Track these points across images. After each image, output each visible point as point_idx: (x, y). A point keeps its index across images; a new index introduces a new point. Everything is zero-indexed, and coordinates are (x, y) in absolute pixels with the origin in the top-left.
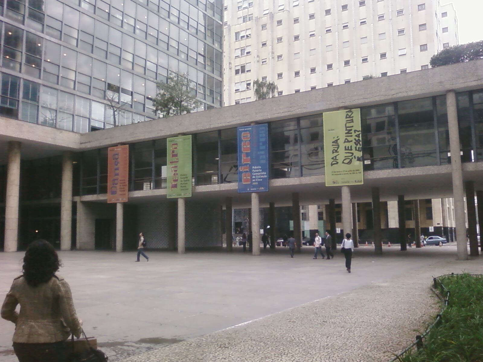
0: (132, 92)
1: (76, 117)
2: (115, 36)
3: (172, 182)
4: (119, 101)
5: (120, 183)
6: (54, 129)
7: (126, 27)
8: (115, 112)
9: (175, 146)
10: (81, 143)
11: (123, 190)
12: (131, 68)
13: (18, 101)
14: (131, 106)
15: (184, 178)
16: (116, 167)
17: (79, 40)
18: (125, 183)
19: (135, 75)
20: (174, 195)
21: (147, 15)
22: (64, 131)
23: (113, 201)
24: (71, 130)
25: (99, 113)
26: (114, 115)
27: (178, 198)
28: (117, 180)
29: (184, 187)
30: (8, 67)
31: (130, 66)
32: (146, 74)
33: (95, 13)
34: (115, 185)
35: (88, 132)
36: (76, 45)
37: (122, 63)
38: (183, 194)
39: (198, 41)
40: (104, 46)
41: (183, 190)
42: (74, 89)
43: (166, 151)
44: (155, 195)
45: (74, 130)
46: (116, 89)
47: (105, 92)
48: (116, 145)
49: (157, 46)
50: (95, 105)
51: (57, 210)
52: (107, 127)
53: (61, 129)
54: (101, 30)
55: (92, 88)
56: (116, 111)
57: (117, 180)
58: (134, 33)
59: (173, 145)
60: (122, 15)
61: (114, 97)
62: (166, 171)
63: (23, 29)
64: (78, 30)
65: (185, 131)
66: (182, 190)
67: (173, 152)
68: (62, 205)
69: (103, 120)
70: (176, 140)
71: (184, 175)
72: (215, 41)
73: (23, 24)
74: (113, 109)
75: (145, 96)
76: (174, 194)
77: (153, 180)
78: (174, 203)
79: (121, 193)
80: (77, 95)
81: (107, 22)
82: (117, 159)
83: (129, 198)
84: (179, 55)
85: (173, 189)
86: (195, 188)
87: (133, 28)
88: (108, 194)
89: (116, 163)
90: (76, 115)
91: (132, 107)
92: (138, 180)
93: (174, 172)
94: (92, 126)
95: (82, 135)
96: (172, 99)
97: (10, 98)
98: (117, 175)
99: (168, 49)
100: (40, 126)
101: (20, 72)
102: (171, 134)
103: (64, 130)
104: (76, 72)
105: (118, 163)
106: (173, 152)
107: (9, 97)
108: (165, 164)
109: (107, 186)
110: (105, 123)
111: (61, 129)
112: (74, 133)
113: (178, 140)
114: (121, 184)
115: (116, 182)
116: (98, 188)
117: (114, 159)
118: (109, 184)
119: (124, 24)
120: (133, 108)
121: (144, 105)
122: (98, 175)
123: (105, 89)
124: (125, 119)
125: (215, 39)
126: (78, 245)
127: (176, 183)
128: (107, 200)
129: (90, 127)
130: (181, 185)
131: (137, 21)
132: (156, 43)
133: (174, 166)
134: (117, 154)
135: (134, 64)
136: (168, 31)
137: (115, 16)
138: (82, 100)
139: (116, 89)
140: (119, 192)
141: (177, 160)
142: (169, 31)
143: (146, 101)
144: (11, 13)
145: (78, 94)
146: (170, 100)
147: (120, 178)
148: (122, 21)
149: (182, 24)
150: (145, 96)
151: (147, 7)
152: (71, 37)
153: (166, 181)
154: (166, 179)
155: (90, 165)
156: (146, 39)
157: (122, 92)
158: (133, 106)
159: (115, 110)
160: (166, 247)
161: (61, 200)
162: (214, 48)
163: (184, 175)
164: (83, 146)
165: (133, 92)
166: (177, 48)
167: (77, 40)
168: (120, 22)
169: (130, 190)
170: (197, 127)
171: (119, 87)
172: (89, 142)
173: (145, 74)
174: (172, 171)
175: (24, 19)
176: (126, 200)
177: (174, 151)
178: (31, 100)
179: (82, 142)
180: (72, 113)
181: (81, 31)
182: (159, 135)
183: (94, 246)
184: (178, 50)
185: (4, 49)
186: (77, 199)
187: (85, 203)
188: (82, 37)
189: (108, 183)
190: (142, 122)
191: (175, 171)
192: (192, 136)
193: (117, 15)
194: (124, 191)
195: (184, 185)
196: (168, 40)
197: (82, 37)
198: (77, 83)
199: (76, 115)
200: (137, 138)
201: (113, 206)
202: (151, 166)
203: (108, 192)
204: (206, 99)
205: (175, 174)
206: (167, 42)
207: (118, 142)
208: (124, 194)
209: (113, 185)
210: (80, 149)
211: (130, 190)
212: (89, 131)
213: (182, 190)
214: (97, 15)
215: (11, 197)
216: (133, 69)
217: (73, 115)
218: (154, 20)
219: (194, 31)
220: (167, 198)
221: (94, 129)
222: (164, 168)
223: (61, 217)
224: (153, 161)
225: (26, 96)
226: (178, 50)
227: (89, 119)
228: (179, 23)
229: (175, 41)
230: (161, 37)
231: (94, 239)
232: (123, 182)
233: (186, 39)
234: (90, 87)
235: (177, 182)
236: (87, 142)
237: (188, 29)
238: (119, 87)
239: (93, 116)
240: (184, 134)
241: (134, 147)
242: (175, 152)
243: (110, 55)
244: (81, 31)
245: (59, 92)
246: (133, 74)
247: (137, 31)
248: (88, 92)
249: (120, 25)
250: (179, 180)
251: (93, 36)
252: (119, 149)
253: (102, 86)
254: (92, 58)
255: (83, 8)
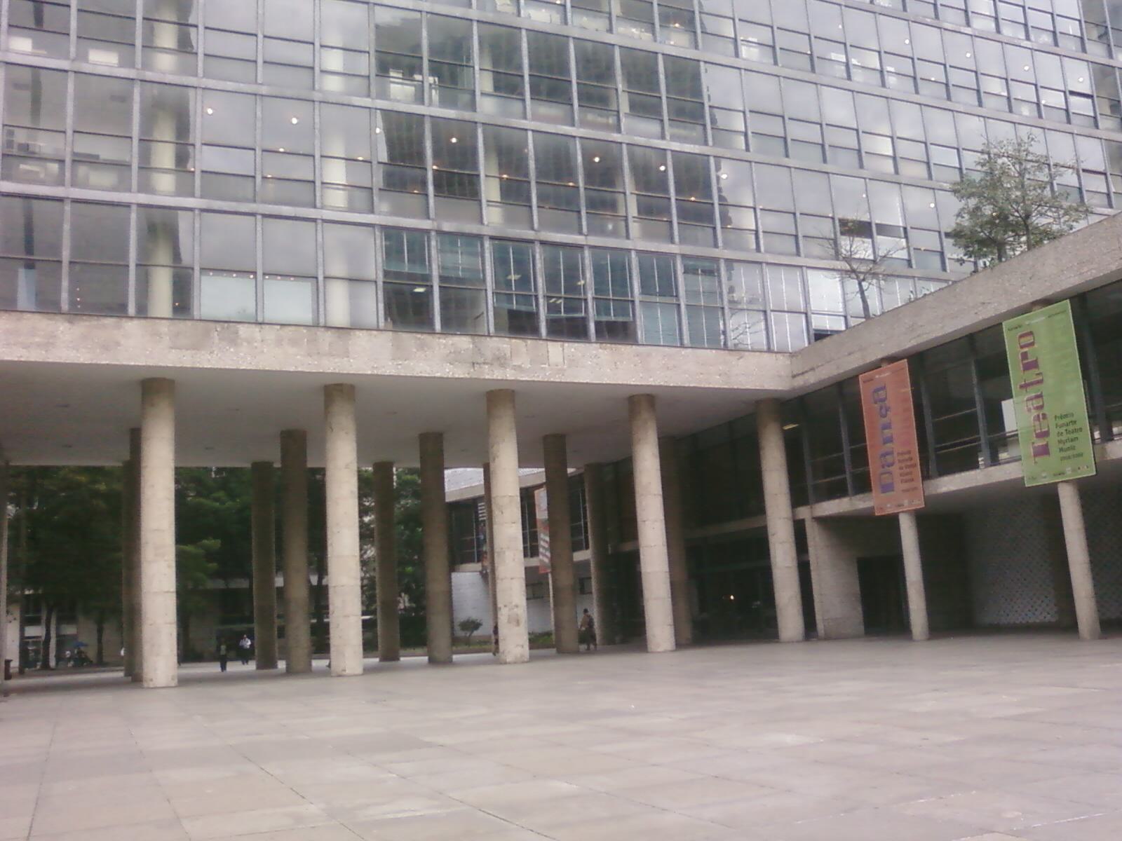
0: (905, 229)
1: (772, 316)
2: (838, 108)
3: (1035, 439)
4: (875, 257)
5: (899, 461)
6: (722, 352)
7: (858, 76)
8: (863, 283)
9: (1028, 340)
10: (794, 377)
11: (908, 477)
12: (892, 170)
13: (633, 302)
14: (909, 261)
15: (1067, 425)
16: (885, 420)
17: (750, 134)
18: (911, 459)
19: (905, 184)
20: (1045, 477)
21: (908, 37)
22: (747, 353)
23: (890, 510)
24: (765, 348)
25: (828, 296)
26: (862, 292)
27: (1056, 483)
28: (890, 453)
29: (1068, 449)
30: (602, 232)
31: (888, 167)
32: (934, 178)
33: (776, 63)
34: (887, 469)
35: (806, 345)
36: (744, 147)
37: (865, 163)
38: (1068, 470)
39: (1064, 63)
40: (813, 133)
41: (1069, 457)
42: (758, 249)
43: (1006, 359)
44: (994, 481)
45: (772, 347)
46: (862, 229)
47: (835, 242)
48: (876, 365)
49: (949, 103)
50: (814, 278)
51: (760, 545)
52: (853, 322)
53: (738, 349)
54: (800, 99)
55: (800, 239)
56: (864, 280)
57: (890, 453)
58: (883, 85)
59: (1021, 336)
60: (843, 51)
61: (854, 246)
62: (1014, 414)
63: (619, 141)
64: (744, 112)
65: (1049, 293)
66: (1063, 458)
67: (1025, 356)
68: (771, 530)
69: (841, 310)
70: (1027, 323)
71: (1066, 416)
72: (1113, 48)
73: (619, 130)
74: (858, 278)
75: (939, 232)
76: (1044, 475)
77: (983, 441)
78: (1048, 499)
79: (906, 486)
80: (768, 264)
81: (812, 77)
82: (883, 400)
83: (927, 499)
84: (1014, 109)
85: (1037, 459)
86: (1104, 450)
87: (878, 75)
88: (874, 494)
89: (883, 411)
90: (772, 311)
91: (910, 265)
92: (946, 448)
93: (1035, 413)
94: (815, 330)
95: (793, 355)
96: (1002, 220)
97: (516, 295)
98: (890, 440)
99: (980, 104)
100: (690, 350)
101: (628, 237)
102: (1010, 308)
103: (749, 351)
104: (755, 209)
105: (887, 410)
106: (1025, 356)
107: (611, 297)
108: (1009, 395)
109: (868, 473)
110: (849, 317)
111: (738, 349)
112: (774, 355)
113: (1033, 322)
114: (903, 465)
115: (889, 459)
116: (849, 480)
117: (876, 403)
118: (874, 467)
119: (853, 70)
120: (914, 266)
121: (942, 254)
122: (846, 447)
123: (835, 233)
124: (887, 297)
125: (1112, 44)
126: (820, 626)
127: (1045, 443)
128: (873, 508)
129: (812, 332)
130: (1061, 446)
131: (883, 55)
132: (945, 96)
133: (1033, 394)
134: (884, 388)
135: (899, 160)
136: (973, 59)
137: (828, 57)
138: (783, 273)
139: (862, 229)
140: (900, 486)
141: (1041, 378)
142: (975, 57)
143: (945, 244)
144: (590, 117)
145: (770, 258)
146: (996, 224)
147: (896, 447)
148: (847, 65)
149: (1008, 31)
150: (939, 232)
151: (904, 15)
152: (735, 131)
153: (1018, 440)
154: (1017, 435)
155: (823, 425)
156: (917, 92)
157: (879, 234)
158: (913, 262)
159: (862, 277)
160: (1053, 620)
161: (765, 520)
162: (1113, 67)
163: (1066, 416)
164: (799, 382)
165: (909, 228)
166: (1005, 94)
167: (746, 135)
168: (843, 68)
169: (926, 476)
170: (1081, 274)
171: (870, 224)
172: (812, 369)
173: (930, 177)
174: (1029, 410)
175: (619, 120)
176: (919, 504)
177: (1026, 353)
178: (661, 295)
179: (795, 373)
180: (761, 308)
181: (751, 111)
182: (981, 318)
183: (862, 628)
184: (1009, 98)
185: (586, 197)
186: (804, 512)
187: (824, 521)
188: (758, 124)
189: (870, 467)
190: (931, 294)
191: (1041, 407)
192: (1071, 302)
193: (833, 54)
194: (912, 480)
195: (1068, 445)
196: (977, 79)
197: (758, 124)
198: (761, 235)
199: (772, 311)
200: (925, 338)
201: (892, 522)
202: (973, 404)
203: (873, 488)
204: (1114, 206)
205: (1038, 416)
206: (976, 87)
207: (880, 356)
208: (915, 489)
209: (883, 467)
210: (794, 390)
211: (926, 476)
212: (809, 343)
213: (1063, 458)
214: (783, 66)
215: (647, 523)
216: (897, 172)
217: (765, 312)
218: (928, 42)
219: (1046, 39)
220: (1027, 486)
221: (820, 336)
222: (1007, 406)
223: (772, 559)
224: (976, 390)
225: (646, 289)
226: (1009, 98)
227: (806, 314)
228: (998, 31)
229: (999, 80)
230: (956, 77)
231: (860, 609)
232: (907, 456)
233: (1026, 68)
234: (796, 236)
235: (1047, 439)
236: (806, 372)
237: (1028, 38)
238: (870, 224)
239: (814, 306)
240: (1046, 302)
241: (924, 364)
242: (1029, 355)
243: (831, 152)
244: (751, 111)
245: (766, 269)
246: (899, 183)
247: (891, 80)
248: (794, 250)
249: (845, 75)
250: (1054, 431)
251: (783, 117)
252: (885, 374)
253: (826, 228)
254: (789, 167)
255: (744, 59)
